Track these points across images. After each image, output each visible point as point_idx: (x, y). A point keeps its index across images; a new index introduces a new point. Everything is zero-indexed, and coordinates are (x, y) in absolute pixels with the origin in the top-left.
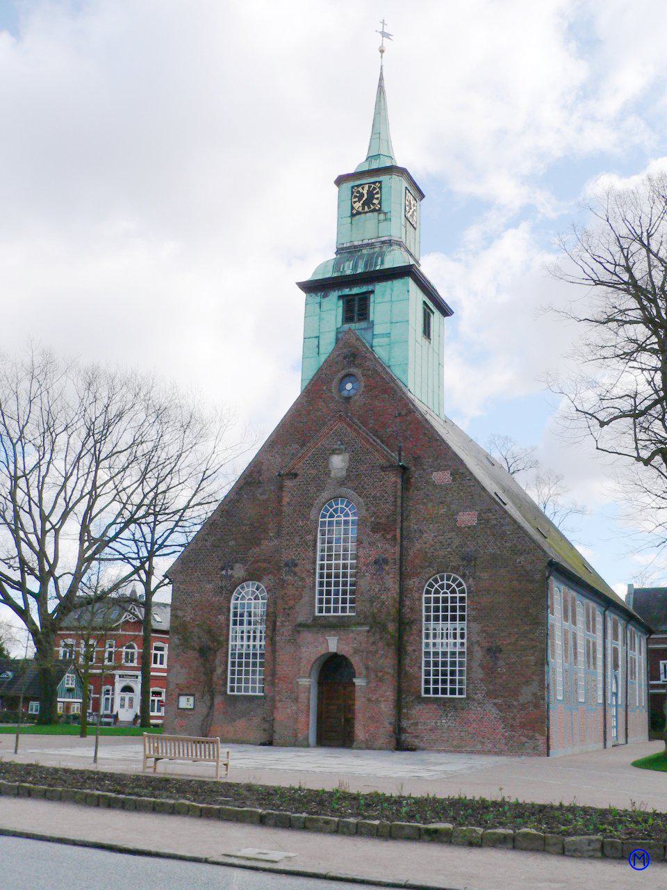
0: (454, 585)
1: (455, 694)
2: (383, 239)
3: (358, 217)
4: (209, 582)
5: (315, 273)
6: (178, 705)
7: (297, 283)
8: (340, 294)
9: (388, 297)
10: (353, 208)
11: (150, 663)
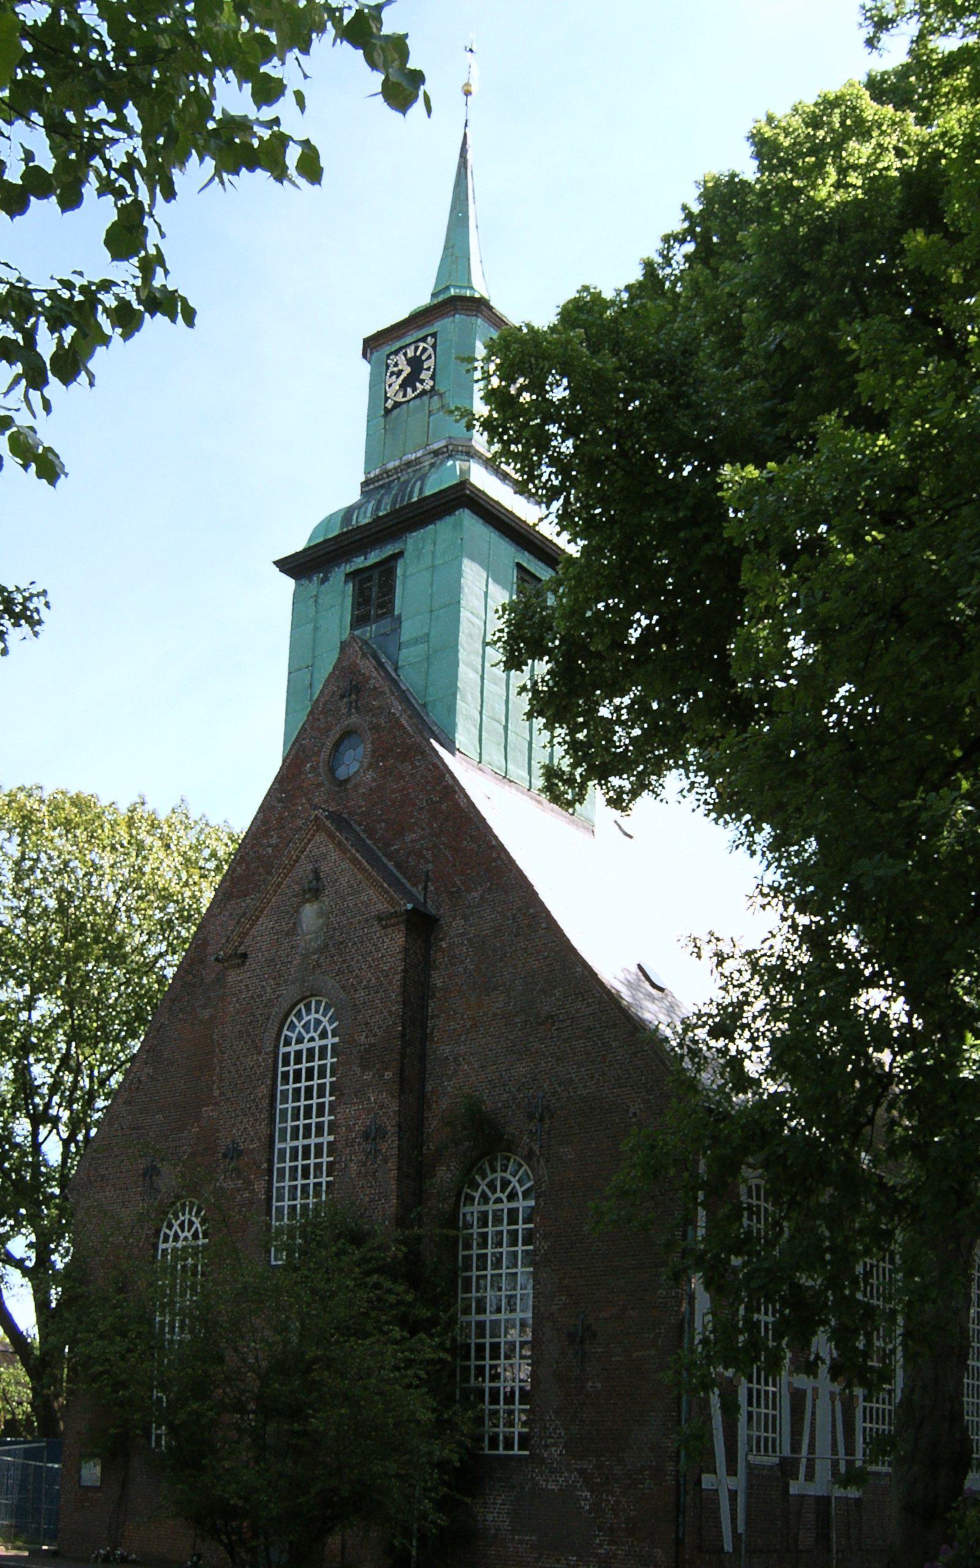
1: (513, 1449)
5: (310, 540)
7: (277, 563)
8: (349, 568)
9: (427, 561)
11: (972, 1452)
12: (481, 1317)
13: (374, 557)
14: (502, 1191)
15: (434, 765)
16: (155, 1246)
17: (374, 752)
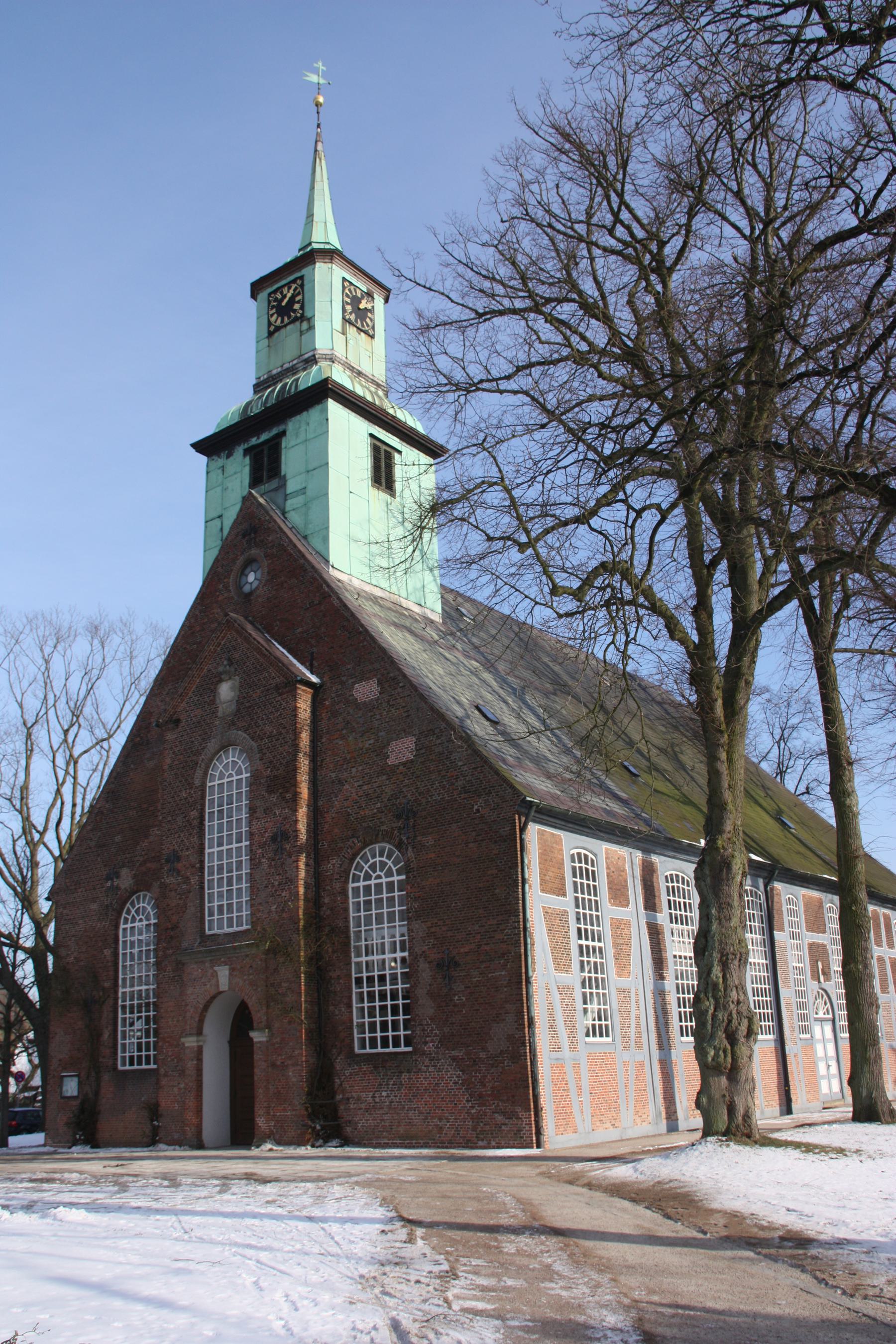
0: (390, 863)
2: (306, 356)
3: (276, 335)
4: (94, 900)
6: (61, 1092)
7: (194, 446)
8: (246, 446)
9: (302, 437)
10: (270, 324)
12: (370, 958)
13: (264, 437)
14: (381, 870)
15: (315, 579)
16: (117, 927)
17: (268, 573)
